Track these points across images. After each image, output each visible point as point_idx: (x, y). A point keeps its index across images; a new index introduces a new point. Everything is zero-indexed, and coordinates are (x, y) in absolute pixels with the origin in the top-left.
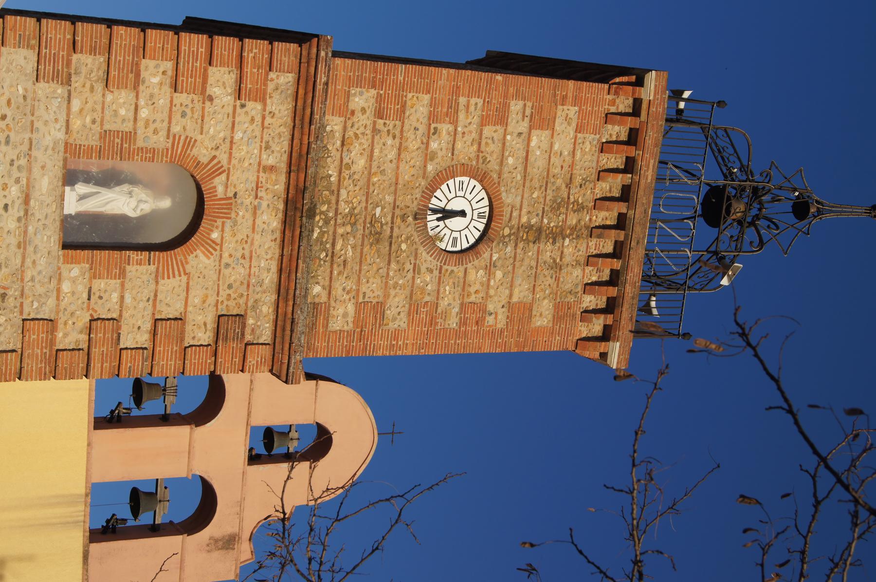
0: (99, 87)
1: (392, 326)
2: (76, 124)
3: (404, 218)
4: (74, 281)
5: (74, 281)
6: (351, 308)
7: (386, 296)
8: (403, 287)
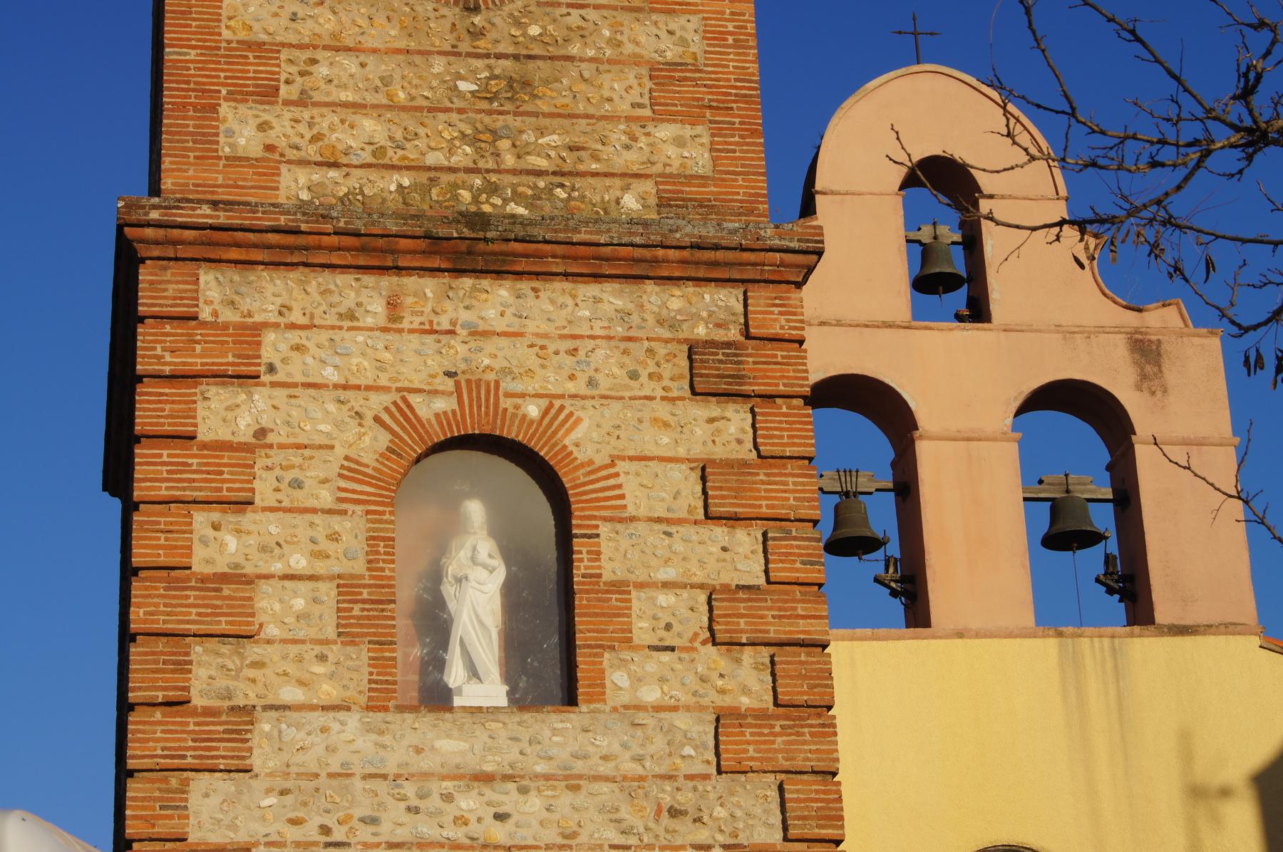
0: (253, 651)
1: (697, 45)
2: (329, 691)
3: (476, 34)
4: (638, 680)
5: (638, 680)
6: (665, 132)
7: (636, 60)
8: (616, 28)
